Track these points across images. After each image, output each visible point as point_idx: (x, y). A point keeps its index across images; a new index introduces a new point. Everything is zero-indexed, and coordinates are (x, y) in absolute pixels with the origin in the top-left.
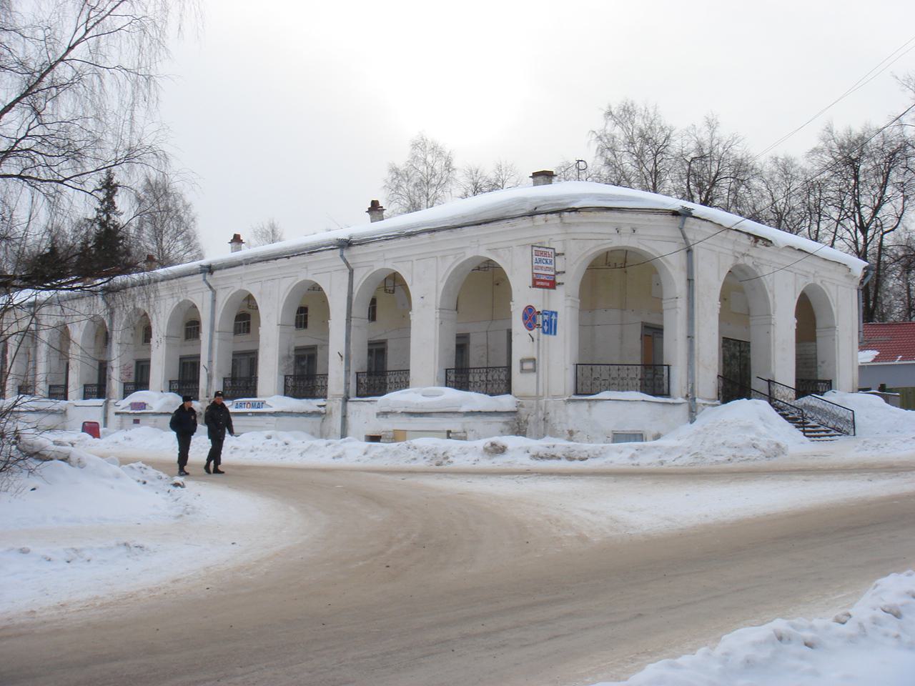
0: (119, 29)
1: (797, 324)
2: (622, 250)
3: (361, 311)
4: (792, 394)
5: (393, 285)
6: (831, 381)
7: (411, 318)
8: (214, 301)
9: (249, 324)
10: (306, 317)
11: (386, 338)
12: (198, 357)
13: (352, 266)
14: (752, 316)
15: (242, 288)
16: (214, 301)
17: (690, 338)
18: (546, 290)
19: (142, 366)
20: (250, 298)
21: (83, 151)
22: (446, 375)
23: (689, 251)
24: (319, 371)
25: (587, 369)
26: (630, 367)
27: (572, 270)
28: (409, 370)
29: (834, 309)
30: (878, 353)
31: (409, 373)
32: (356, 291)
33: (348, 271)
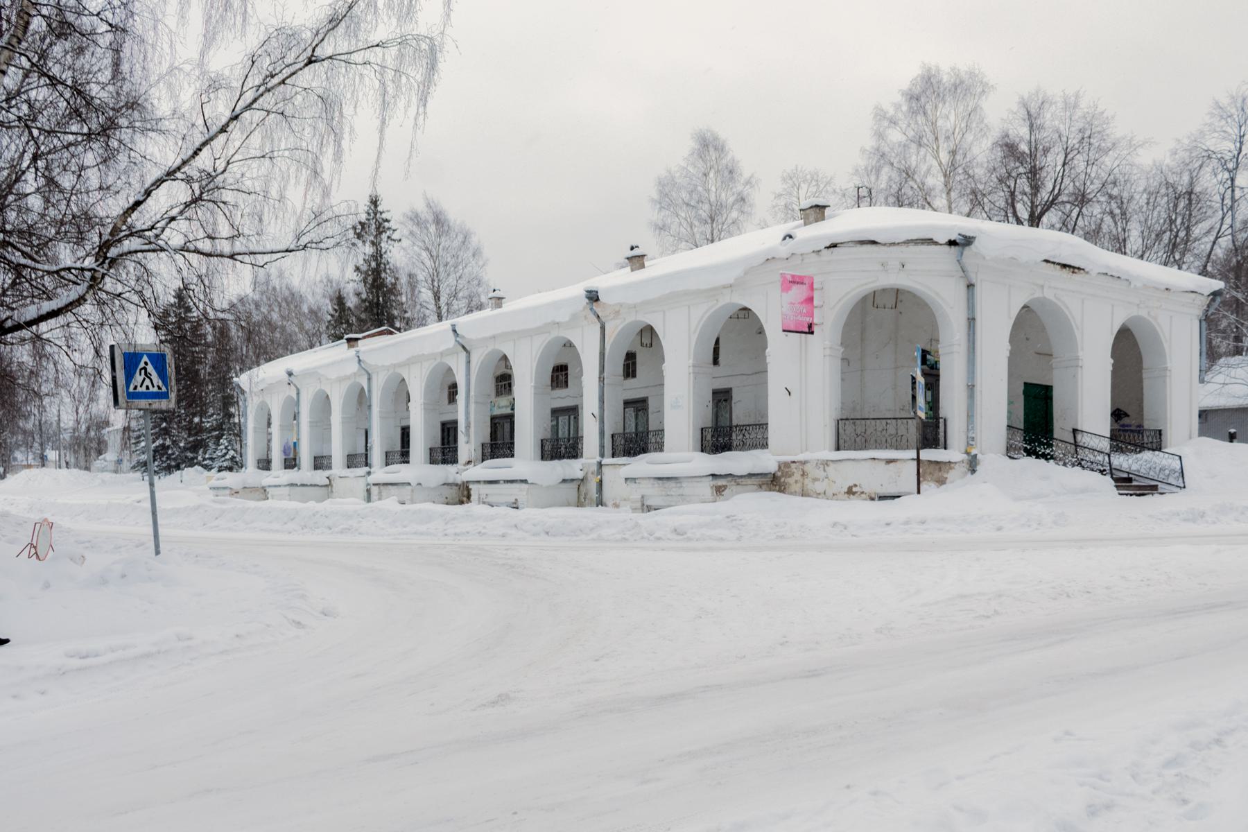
0: (330, 58)
1: (1113, 365)
2: (892, 289)
3: (616, 365)
4: (1105, 445)
5: (648, 335)
6: (1160, 431)
7: (768, 361)
8: (469, 362)
9: (510, 385)
10: (634, 364)
11: (646, 395)
12: (456, 422)
13: (603, 320)
14: (1056, 358)
15: (638, 319)
16: (469, 362)
17: (971, 388)
18: (804, 335)
19: (449, 429)
20: (569, 345)
21: (43, 419)
22: (702, 433)
23: (970, 286)
24: (652, 426)
25: (849, 427)
26: (889, 421)
27: (830, 317)
28: (663, 430)
29: (1166, 346)
30: (202, 449)
31: (767, 429)
32: (608, 347)
33: (599, 326)
